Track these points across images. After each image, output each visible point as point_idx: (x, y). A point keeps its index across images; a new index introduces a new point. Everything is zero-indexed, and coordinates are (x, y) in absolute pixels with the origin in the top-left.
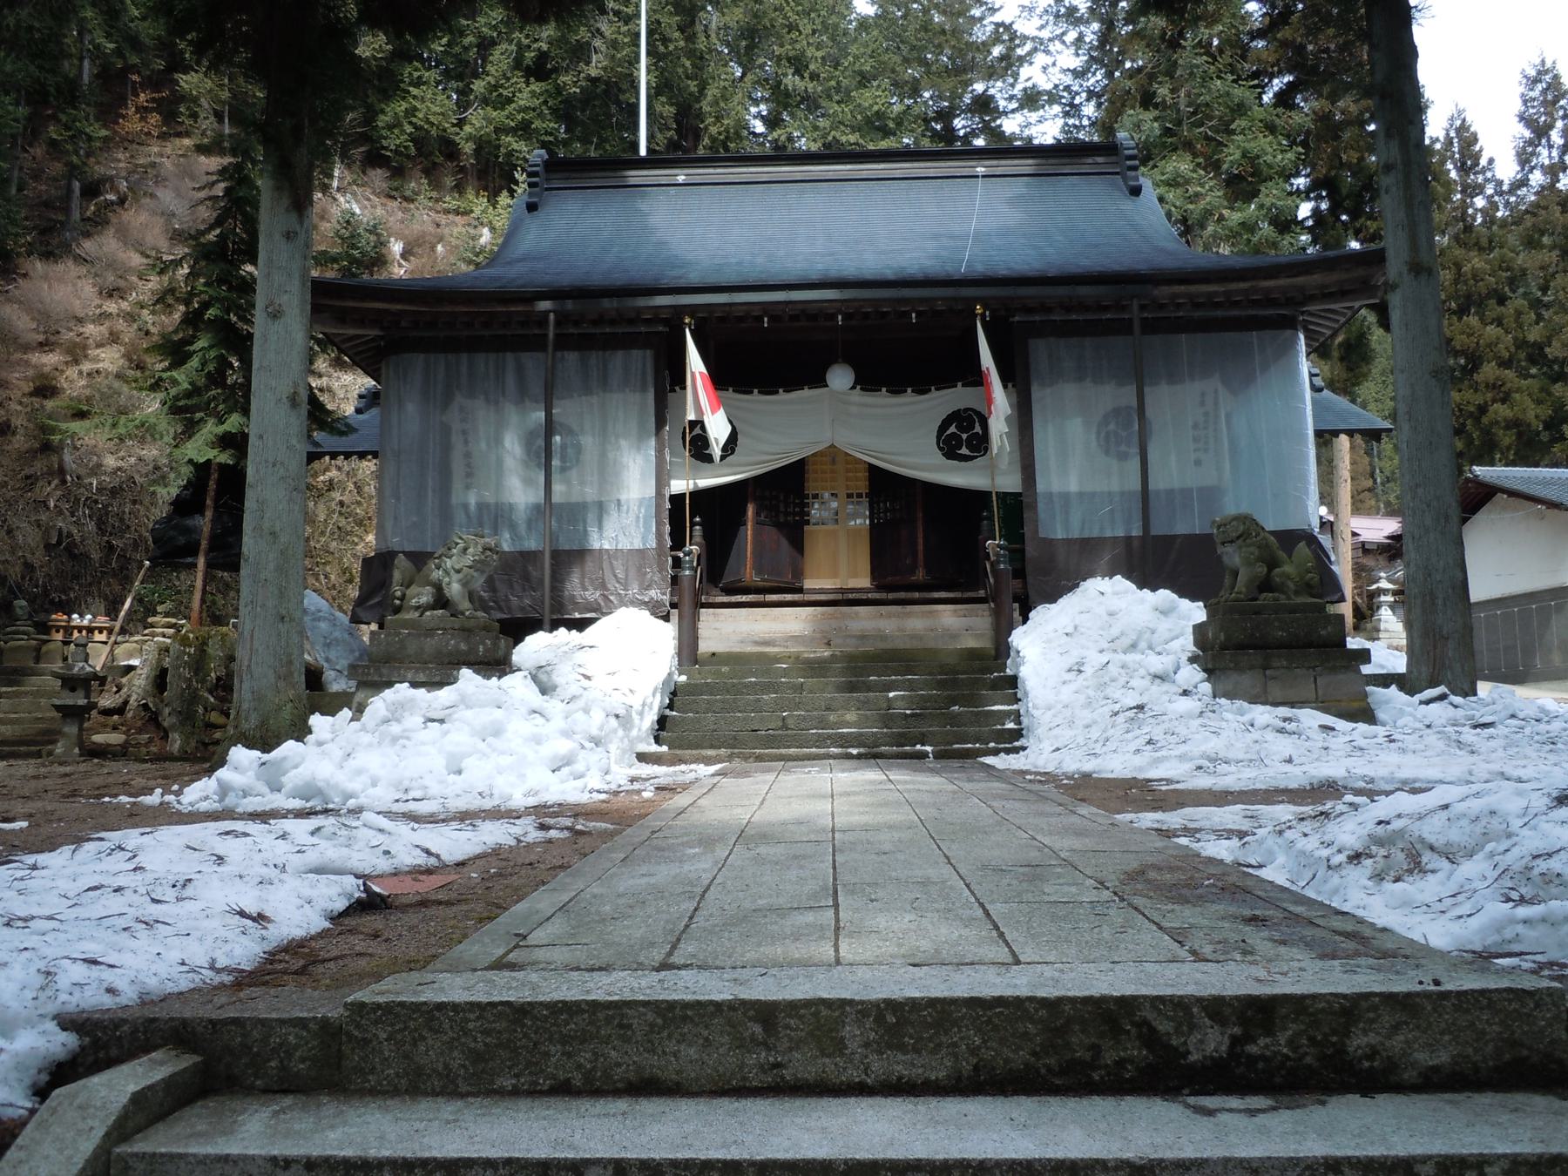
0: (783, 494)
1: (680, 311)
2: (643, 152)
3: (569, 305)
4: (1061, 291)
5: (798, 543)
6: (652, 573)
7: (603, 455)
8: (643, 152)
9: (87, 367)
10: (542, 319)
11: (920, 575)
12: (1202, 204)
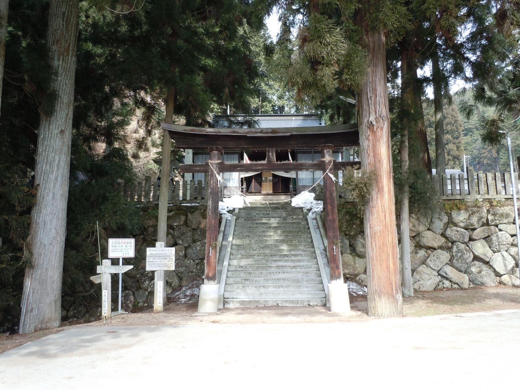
2: (229, 114)
5: (261, 186)
8: (229, 114)
11: (280, 191)
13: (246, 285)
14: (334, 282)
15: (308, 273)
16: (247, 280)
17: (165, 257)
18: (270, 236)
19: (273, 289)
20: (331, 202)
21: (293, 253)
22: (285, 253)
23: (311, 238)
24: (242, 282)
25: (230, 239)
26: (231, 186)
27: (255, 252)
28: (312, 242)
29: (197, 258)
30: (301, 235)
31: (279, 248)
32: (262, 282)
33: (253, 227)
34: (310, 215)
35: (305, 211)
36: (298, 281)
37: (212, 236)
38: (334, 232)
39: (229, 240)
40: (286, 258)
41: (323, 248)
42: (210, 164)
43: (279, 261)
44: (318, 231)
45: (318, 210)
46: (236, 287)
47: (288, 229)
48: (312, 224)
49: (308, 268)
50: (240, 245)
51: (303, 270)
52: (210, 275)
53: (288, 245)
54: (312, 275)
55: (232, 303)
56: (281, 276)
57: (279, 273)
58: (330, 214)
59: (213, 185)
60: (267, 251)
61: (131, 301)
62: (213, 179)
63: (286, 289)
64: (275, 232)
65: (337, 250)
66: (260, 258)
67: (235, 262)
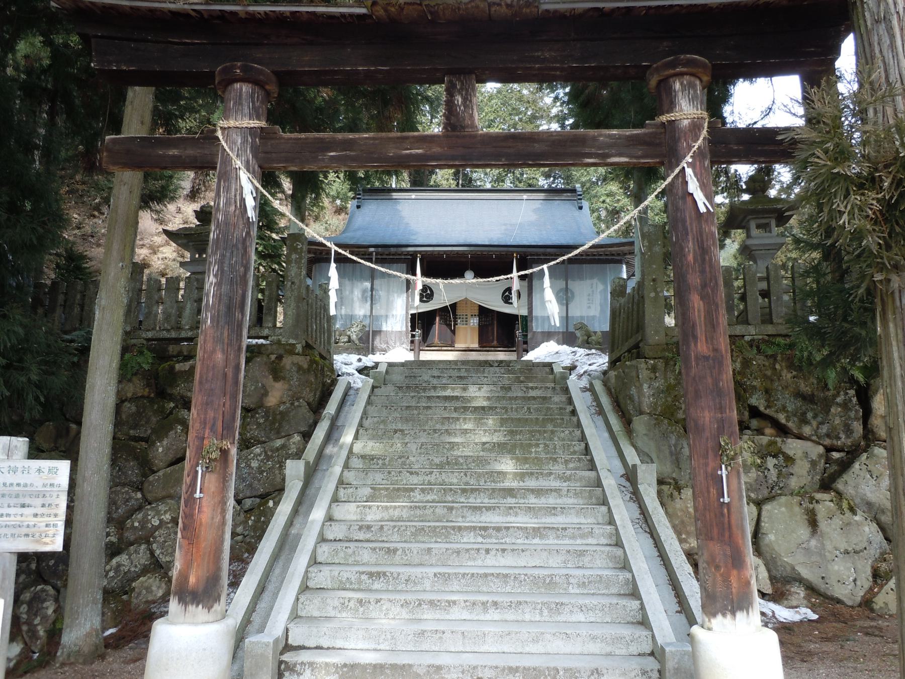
0: (449, 313)
1: (416, 252)
3: (380, 249)
4: (542, 250)
5: (454, 332)
6: (404, 339)
7: (388, 299)
9: (160, 256)
10: (371, 254)
12: (620, 204)
13: (372, 597)
14: (718, 622)
15: (582, 554)
16: (378, 575)
17: (21, 497)
18: (465, 432)
19: (466, 615)
20: (704, 286)
21: (531, 483)
22: (507, 484)
23: (583, 438)
24: (360, 582)
25: (347, 438)
26: (389, 329)
27: (415, 479)
28: (587, 450)
29: (248, 494)
30: (553, 432)
31: (488, 468)
32: (427, 585)
33: (417, 408)
34: (573, 381)
35: (557, 369)
36: (549, 584)
37: (211, 414)
38: (721, 409)
39: (342, 440)
40: (511, 500)
41: (623, 472)
42: (219, 134)
43: (488, 509)
44: (600, 421)
45: (593, 367)
46: (336, 603)
47: (514, 415)
48: (582, 402)
49: (582, 536)
50: (372, 458)
51: (567, 541)
52: (192, 580)
53: (517, 459)
54: (598, 563)
55: (308, 672)
56: (495, 562)
57: (487, 551)
58: (700, 331)
59: (226, 214)
60: (453, 479)
61: (45, 618)
62: (228, 190)
63: (510, 616)
64: (479, 421)
65: (734, 482)
66: (430, 497)
67: (348, 512)
